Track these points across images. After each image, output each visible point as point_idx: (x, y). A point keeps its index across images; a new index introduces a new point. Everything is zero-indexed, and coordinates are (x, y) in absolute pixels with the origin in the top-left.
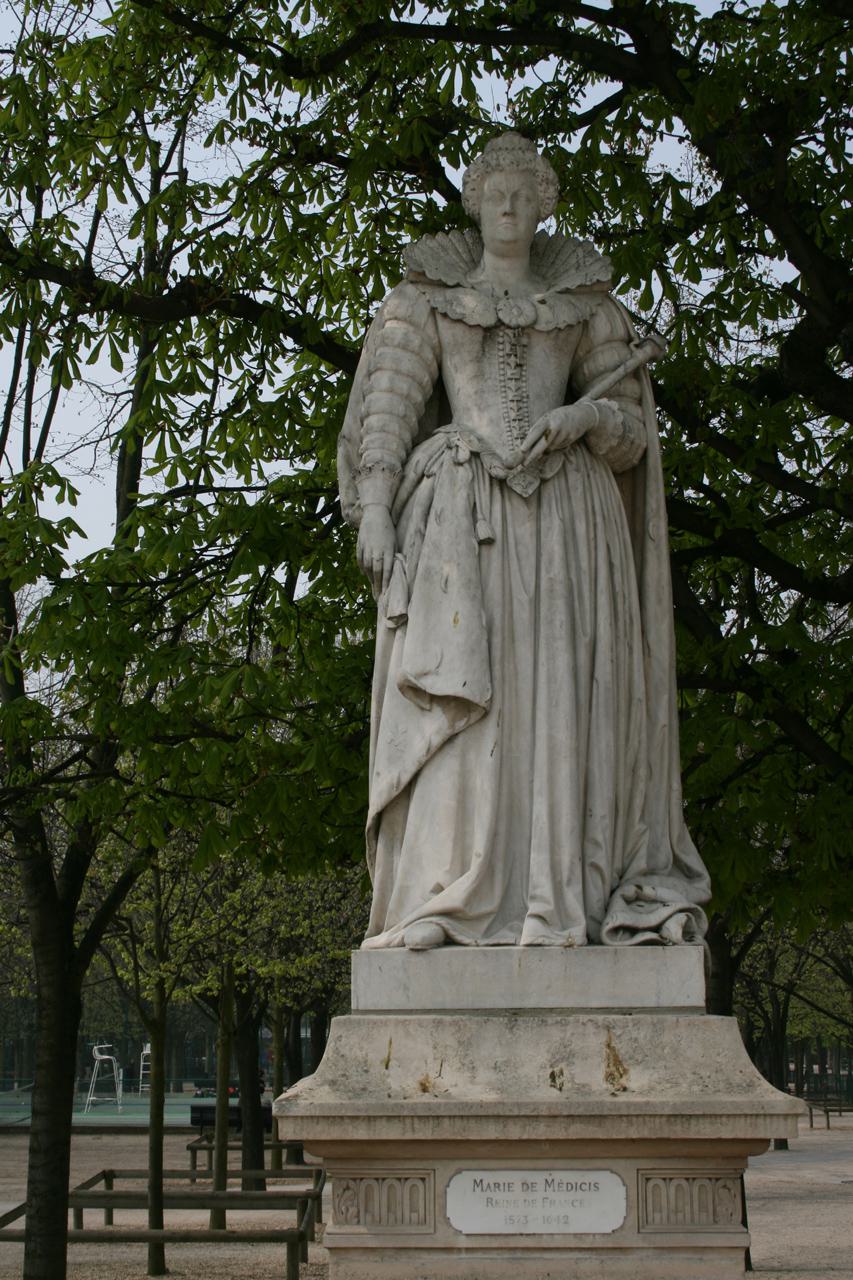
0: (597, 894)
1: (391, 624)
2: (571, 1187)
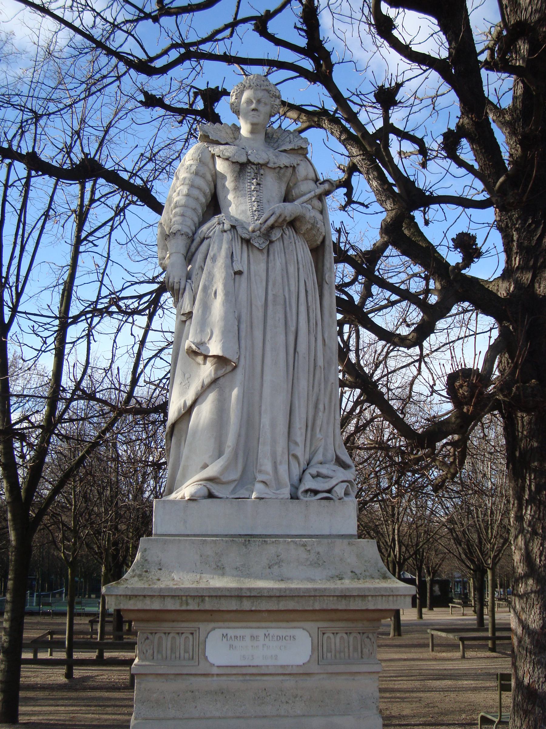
0: (296, 472)
2: (279, 638)
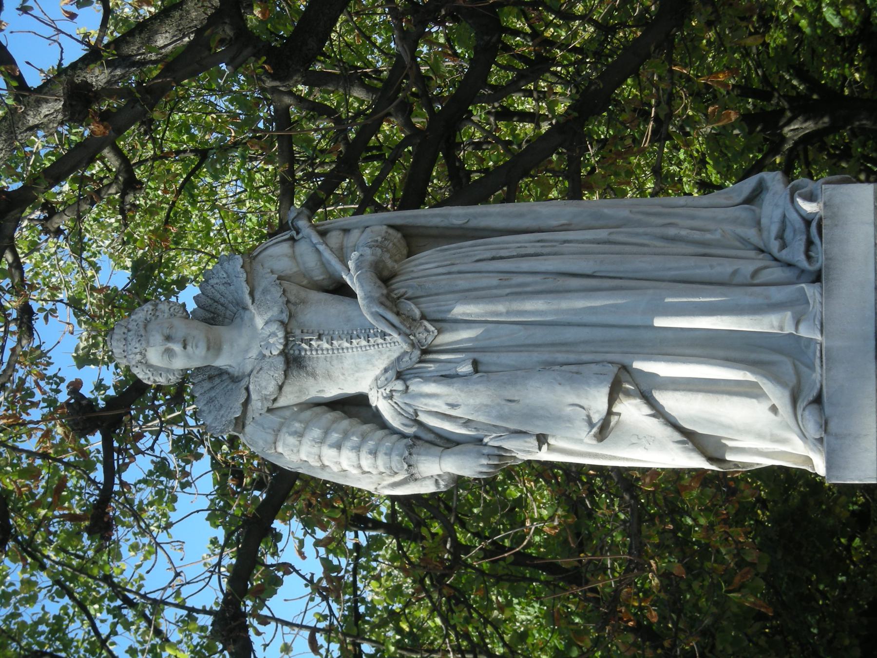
0: (777, 273)
1: (545, 447)
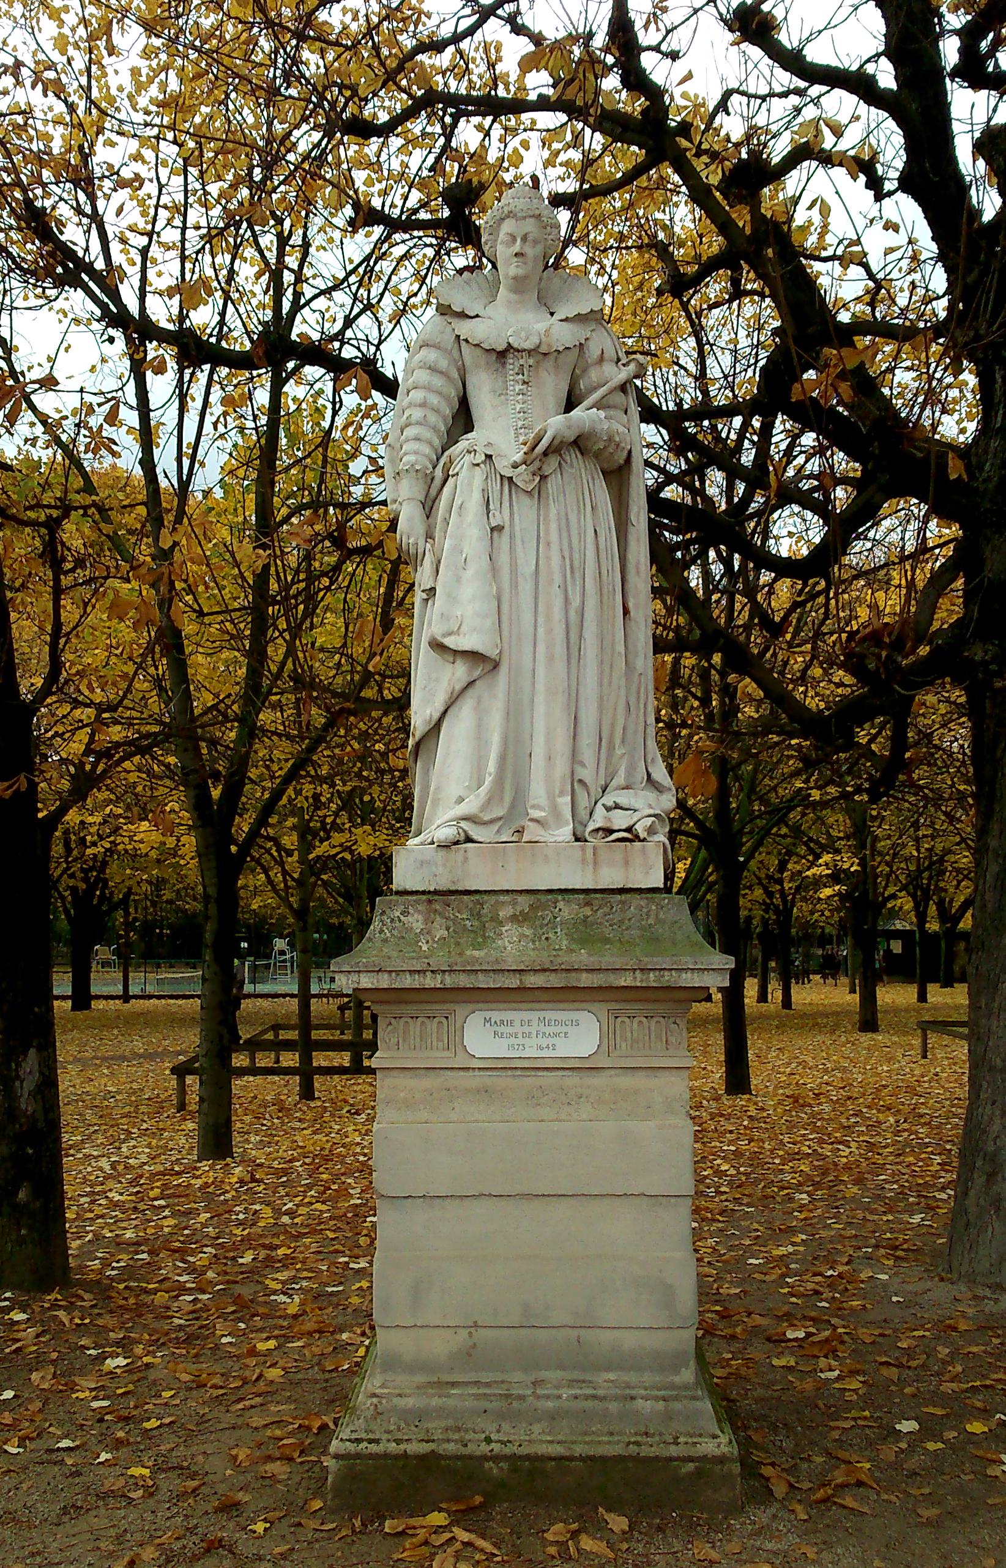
1: (425, 596)
